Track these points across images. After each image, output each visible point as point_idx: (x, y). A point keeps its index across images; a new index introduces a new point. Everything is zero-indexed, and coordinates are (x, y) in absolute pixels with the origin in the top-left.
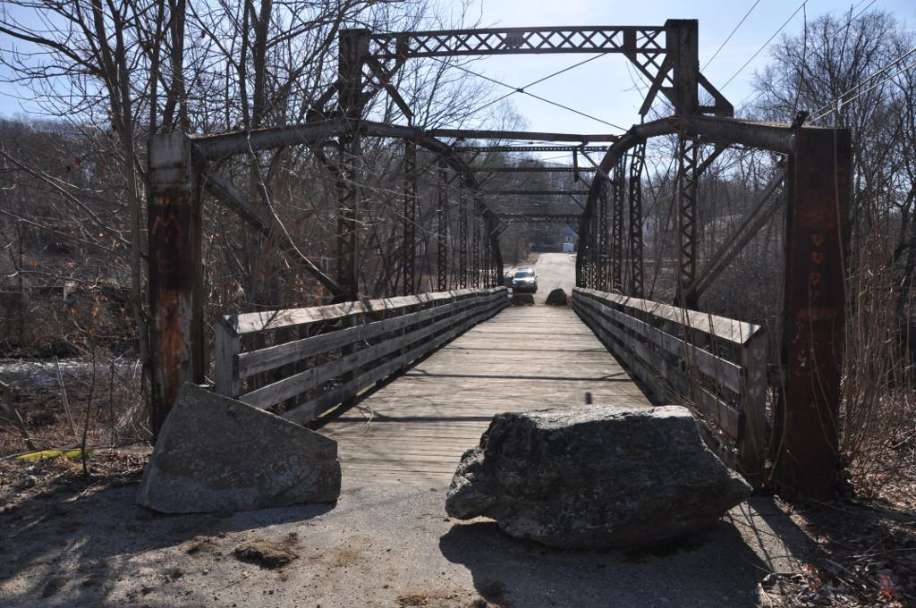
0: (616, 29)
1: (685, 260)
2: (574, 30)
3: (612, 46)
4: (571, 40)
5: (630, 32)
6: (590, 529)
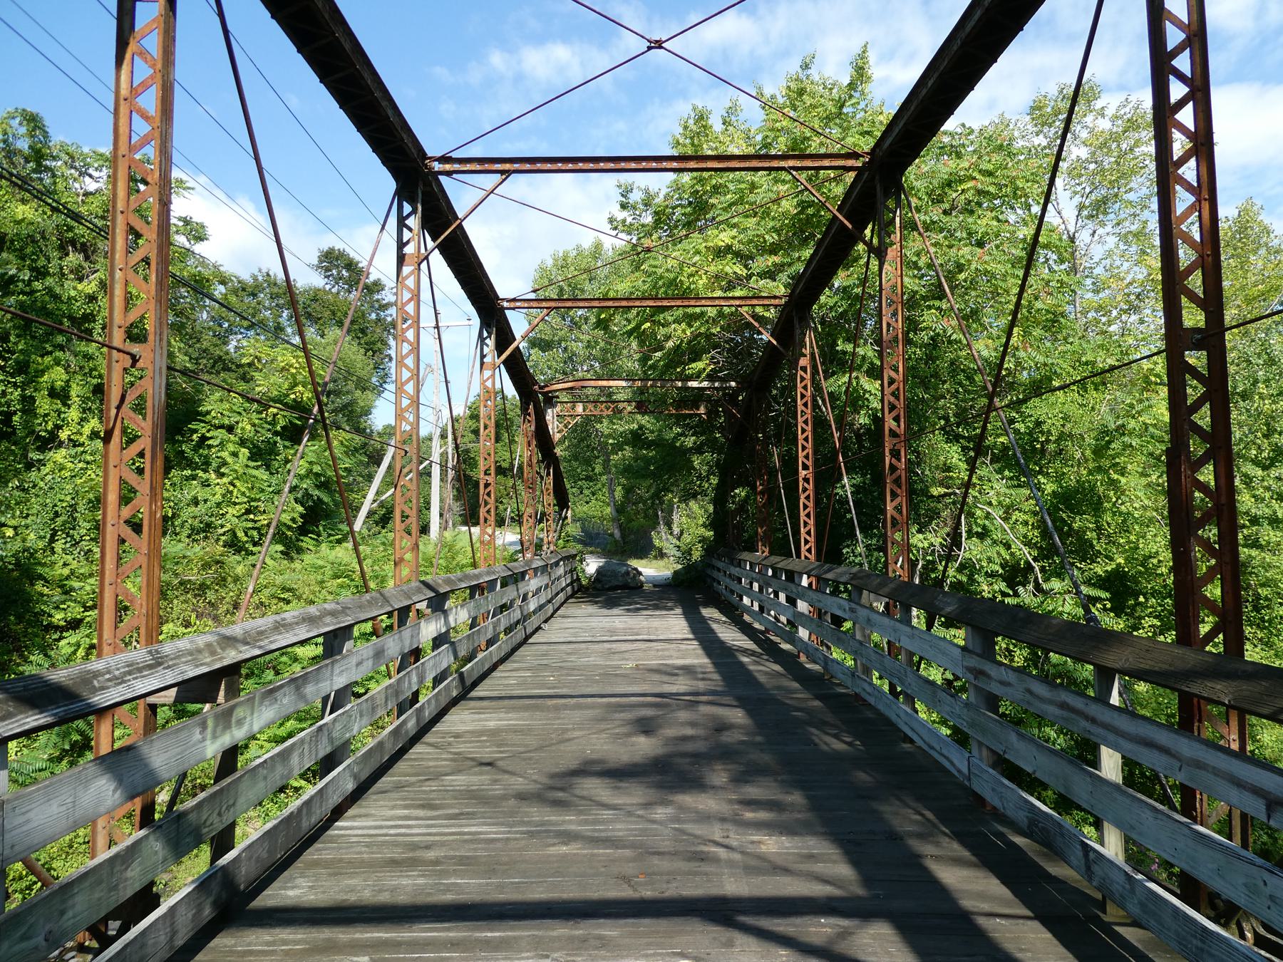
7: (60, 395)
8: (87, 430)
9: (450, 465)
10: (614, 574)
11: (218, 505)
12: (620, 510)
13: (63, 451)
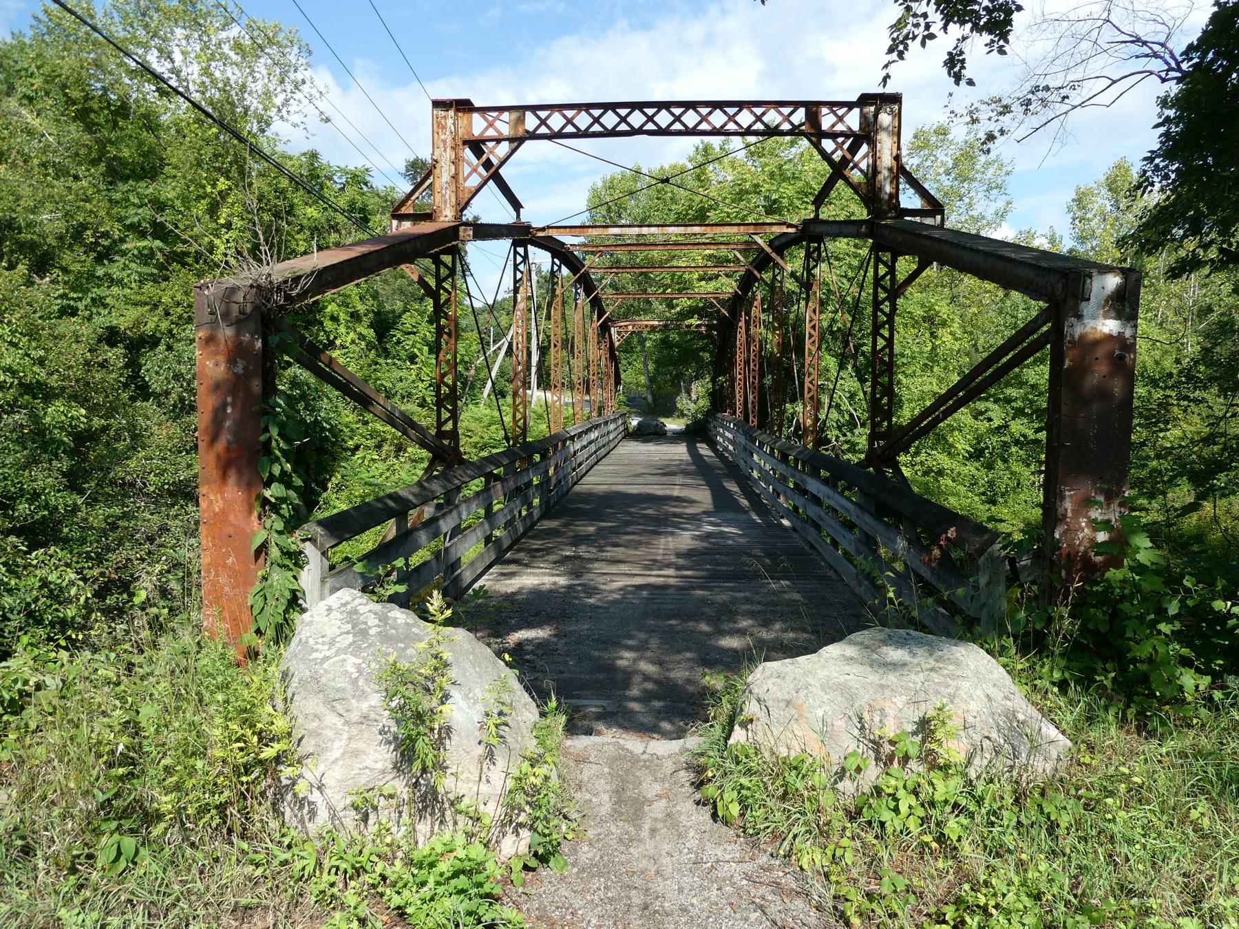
0: (796, 105)
1: (882, 295)
2: (741, 105)
3: (628, 128)
4: (753, 119)
5: (813, 109)
6: (557, 700)
7: (334, 319)
8: (349, 339)
9: (645, 230)
10: (649, 425)
11: (413, 382)
12: (652, 380)
13: (338, 352)
